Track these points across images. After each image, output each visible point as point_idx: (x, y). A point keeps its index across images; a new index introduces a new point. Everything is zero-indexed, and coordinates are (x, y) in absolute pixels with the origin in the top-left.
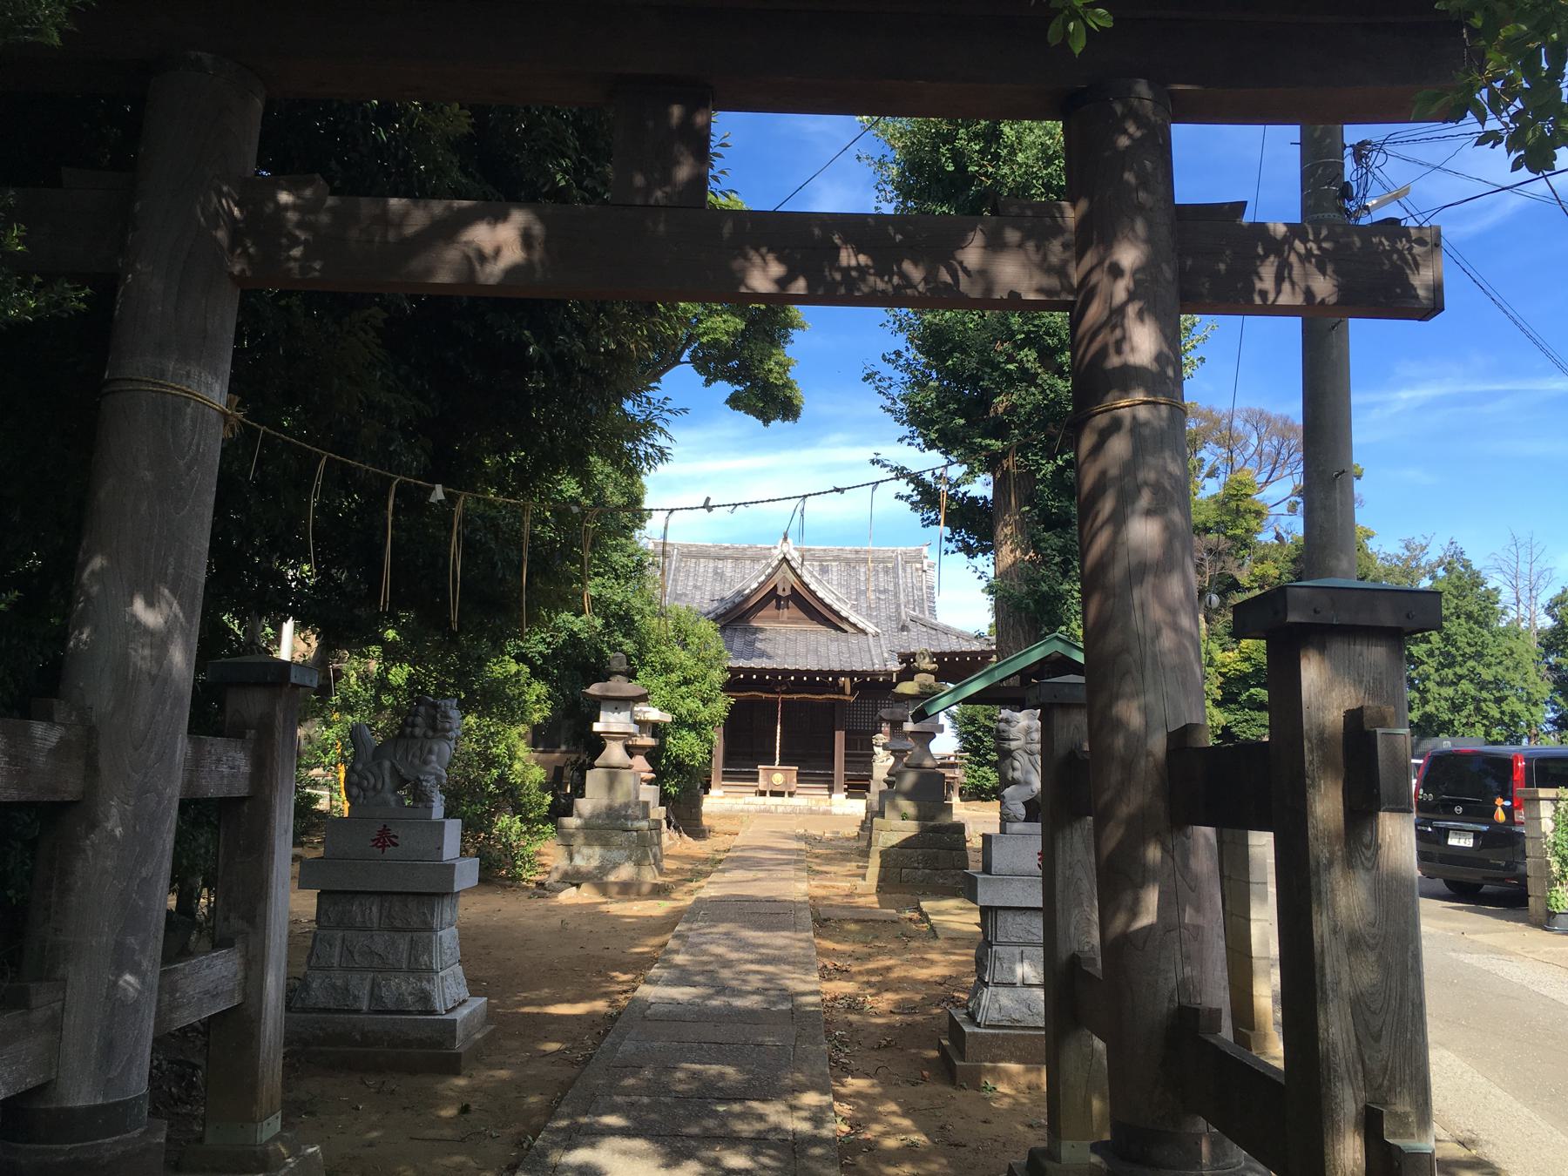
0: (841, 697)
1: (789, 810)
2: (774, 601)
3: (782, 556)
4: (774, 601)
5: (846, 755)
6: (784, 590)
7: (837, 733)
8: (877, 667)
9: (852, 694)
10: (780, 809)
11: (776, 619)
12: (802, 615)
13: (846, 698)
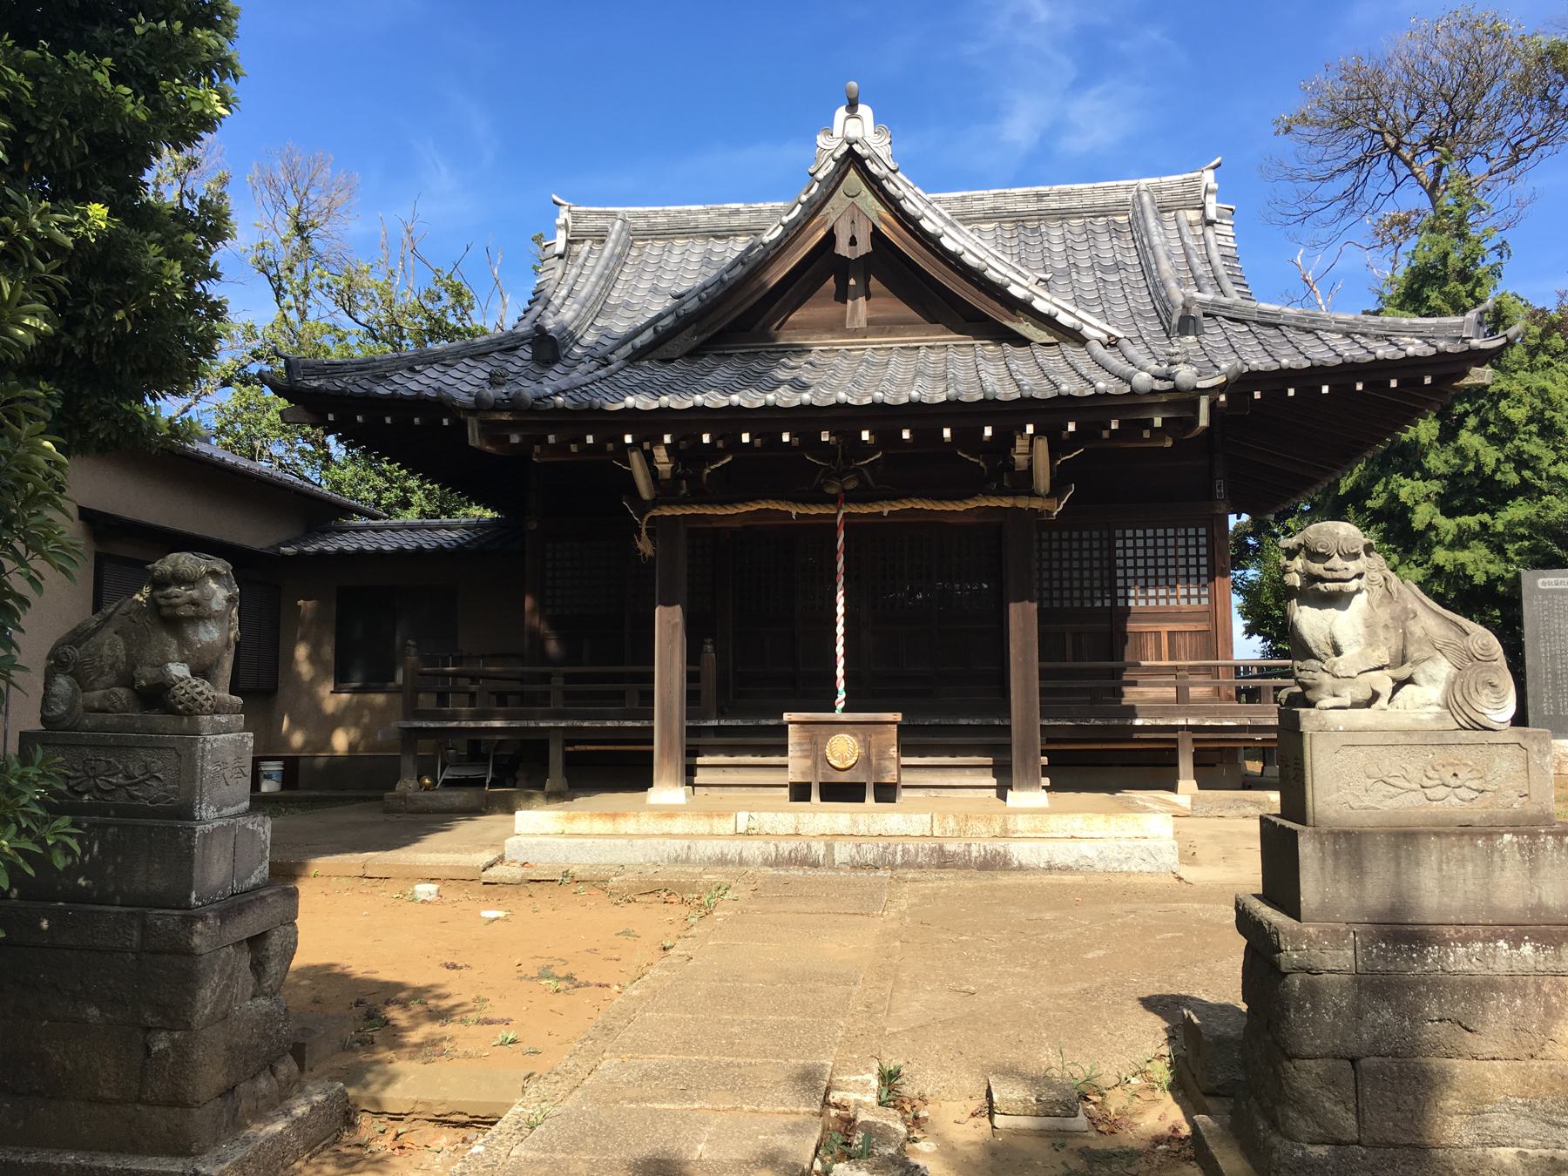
0: (1023, 503)
1: (870, 852)
2: (831, 282)
3: (846, 147)
4: (831, 282)
5: (1044, 674)
6: (853, 242)
7: (1015, 609)
8: (1142, 379)
9: (1056, 490)
10: (843, 852)
11: (837, 327)
12: (904, 310)
13: (1037, 504)
